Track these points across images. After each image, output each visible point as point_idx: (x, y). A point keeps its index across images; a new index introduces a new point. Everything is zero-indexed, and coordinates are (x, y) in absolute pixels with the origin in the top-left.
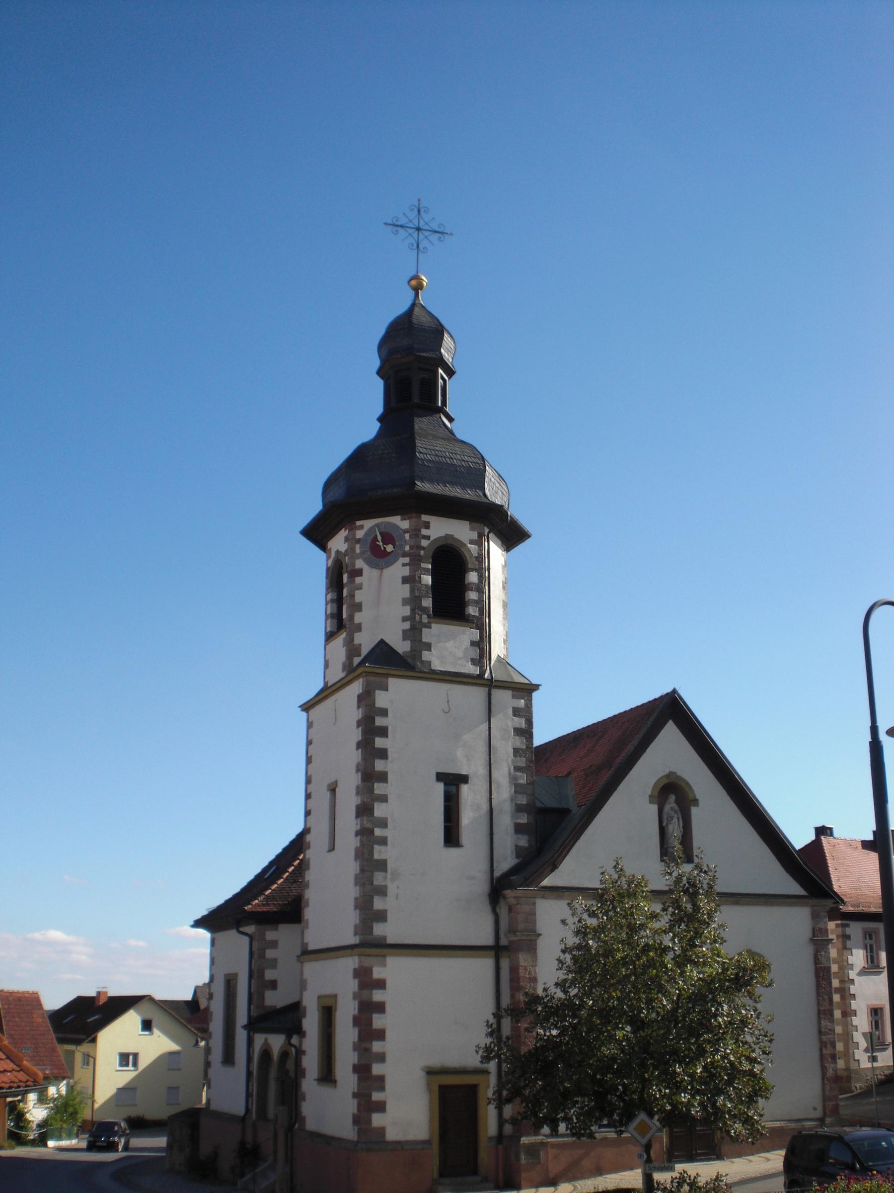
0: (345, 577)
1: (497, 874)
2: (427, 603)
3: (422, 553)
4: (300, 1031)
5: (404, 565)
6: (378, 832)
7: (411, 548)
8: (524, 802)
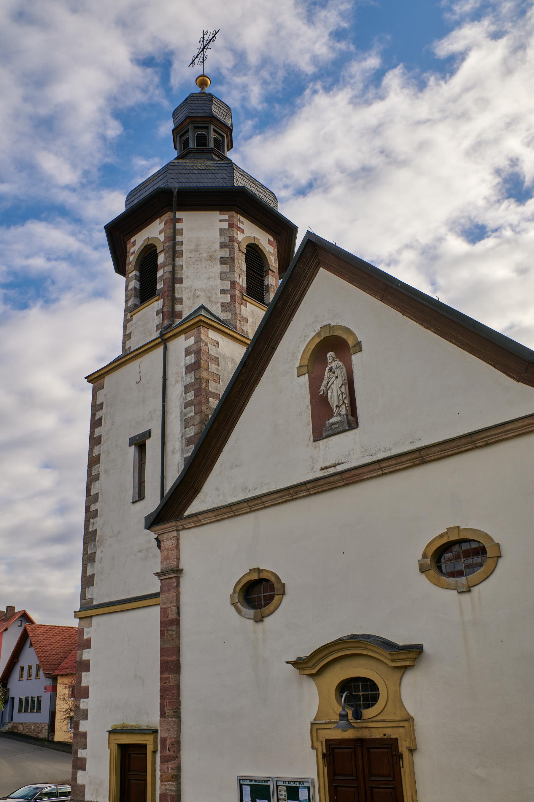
8: (192, 434)
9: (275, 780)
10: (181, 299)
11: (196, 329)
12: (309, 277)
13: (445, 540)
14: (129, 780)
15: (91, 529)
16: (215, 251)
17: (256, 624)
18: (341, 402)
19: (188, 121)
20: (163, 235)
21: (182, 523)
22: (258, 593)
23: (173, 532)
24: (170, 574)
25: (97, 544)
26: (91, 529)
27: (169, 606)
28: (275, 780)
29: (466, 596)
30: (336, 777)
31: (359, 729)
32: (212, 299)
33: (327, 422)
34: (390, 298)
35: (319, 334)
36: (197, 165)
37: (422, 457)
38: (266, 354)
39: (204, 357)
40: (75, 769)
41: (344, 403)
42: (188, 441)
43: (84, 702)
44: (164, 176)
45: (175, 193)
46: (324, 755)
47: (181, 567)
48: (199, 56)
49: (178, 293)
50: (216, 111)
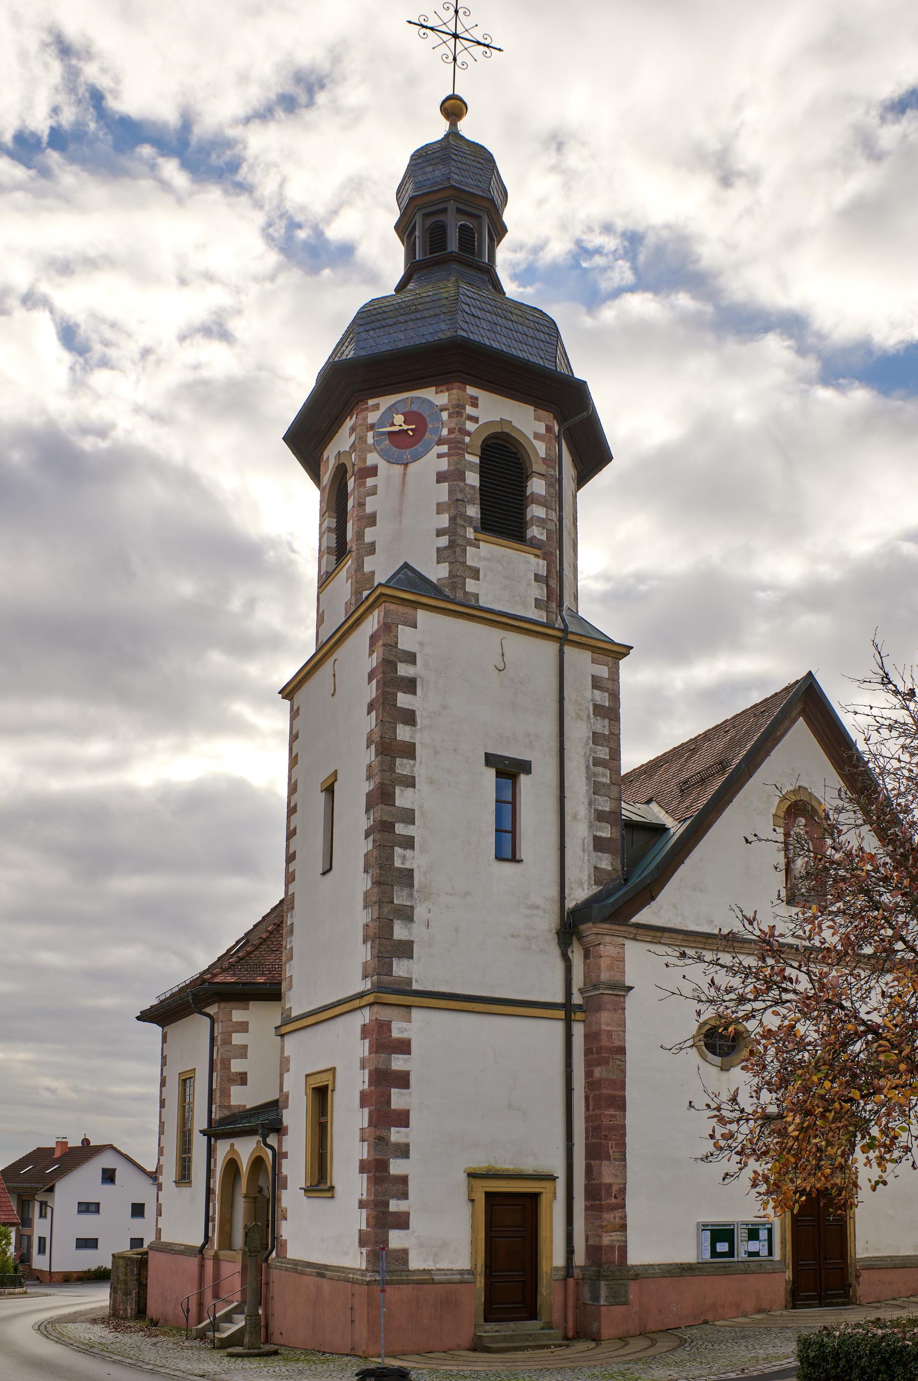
0: (351, 484)
1: (570, 904)
2: (473, 511)
3: (467, 439)
4: (278, 1128)
5: (440, 456)
6: (400, 829)
7: (450, 431)
8: (607, 809)
25: (415, 894)
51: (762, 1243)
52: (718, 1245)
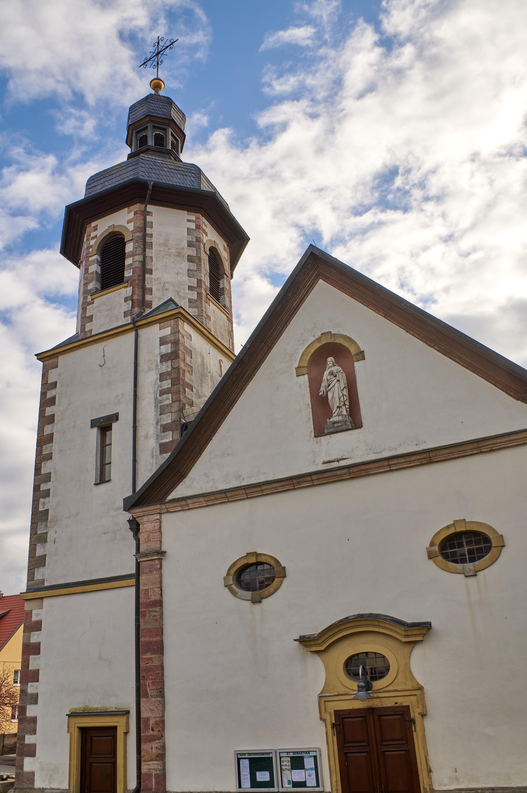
8: (170, 421)
9: (278, 752)
10: (151, 290)
11: (173, 321)
12: (308, 286)
13: (452, 531)
14: (91, 763)
15: (41, 509)
16: (183, 248)
17: (253, 606)
18: (342, 404)
19: (147, 119)
20: (132, 224)
21: (167, 507)
22: (255, 577)
23: (156, 515)
24: (153, 555)
25: (49, 524)
26: (41, 509)
27: (151, 587)
28: (278, 752)
29: (472, 580)
30: (347, 745)
31: (370, 700)
32: (180, 294)
33: (328, 421)
34: (394, 315)
35: (319, 340)
36: (166, 163)
37: (430, 458)
38: (262, 353)
39: (181, 348)
40: (21, 756)
41: (345, 404)
42: (164, 428)
43: (32, 686)
44: (134, 167)
45: (150, 187)
46: (333, 725)
47: (163, 549)
48: (153, 59)
49: (148, 284)
50: (174, 114)
51: (308, 773)
52: (258, 773)
